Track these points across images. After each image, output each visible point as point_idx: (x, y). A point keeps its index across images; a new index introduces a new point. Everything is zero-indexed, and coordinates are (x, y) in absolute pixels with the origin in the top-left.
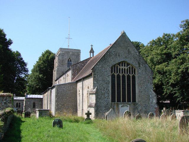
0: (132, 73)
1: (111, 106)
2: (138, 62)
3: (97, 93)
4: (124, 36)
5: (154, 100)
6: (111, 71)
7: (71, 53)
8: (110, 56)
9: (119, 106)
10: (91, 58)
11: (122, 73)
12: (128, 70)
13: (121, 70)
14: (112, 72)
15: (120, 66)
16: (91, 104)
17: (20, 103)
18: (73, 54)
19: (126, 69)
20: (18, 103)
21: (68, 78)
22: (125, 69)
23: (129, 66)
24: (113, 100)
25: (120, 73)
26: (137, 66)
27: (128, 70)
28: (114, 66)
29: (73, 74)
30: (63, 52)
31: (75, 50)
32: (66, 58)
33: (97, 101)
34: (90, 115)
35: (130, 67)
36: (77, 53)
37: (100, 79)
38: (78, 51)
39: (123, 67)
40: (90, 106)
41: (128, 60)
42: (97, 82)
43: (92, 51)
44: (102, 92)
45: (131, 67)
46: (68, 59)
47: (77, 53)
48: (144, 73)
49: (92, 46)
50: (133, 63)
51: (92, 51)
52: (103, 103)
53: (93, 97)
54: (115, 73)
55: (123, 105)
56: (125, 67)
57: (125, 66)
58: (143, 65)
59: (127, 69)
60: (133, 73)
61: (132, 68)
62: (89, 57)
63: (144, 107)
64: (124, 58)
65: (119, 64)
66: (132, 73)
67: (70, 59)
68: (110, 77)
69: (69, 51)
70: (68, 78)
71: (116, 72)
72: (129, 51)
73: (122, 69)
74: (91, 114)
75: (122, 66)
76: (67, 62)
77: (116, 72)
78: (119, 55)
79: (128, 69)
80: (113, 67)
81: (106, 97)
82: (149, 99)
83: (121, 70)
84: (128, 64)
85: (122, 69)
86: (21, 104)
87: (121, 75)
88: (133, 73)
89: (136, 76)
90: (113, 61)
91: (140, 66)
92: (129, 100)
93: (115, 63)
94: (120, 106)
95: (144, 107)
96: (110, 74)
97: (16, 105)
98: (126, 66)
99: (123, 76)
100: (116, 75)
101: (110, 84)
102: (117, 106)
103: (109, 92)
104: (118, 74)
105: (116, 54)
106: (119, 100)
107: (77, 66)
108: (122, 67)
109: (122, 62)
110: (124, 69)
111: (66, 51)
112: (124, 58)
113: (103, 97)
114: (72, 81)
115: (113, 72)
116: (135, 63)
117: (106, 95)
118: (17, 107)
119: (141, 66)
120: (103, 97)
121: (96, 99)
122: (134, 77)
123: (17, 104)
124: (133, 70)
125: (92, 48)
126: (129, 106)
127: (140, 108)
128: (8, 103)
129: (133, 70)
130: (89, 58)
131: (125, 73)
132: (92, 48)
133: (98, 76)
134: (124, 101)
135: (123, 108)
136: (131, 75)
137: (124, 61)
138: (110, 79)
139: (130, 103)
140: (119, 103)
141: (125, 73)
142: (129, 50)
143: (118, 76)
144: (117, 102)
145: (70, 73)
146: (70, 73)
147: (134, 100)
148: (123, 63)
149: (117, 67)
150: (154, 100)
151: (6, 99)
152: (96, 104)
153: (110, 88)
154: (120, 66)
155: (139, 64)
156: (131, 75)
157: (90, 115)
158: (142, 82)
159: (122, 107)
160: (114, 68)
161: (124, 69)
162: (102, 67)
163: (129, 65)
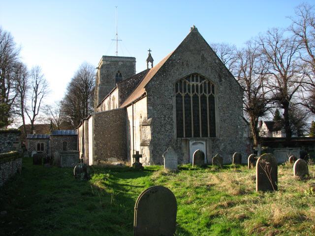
0: (209, 92)
1: (176, 144)
2: (219, 75)
3: (152, 124)
4: (195, 36)
5: (244, 132)
6: (175, 90)
7: (120, 63)
8: (173, 66)
9: (189, 143)
10: (148, 70)
11: (193, 92)
12: (203, 86)
13: (191, 87)
14: (177, 91)
15: (189, 81)
16: (145, 141)
17: (42, 144)
18: (123, 65)
19: (199, 85)
20: (41, 143)
21: (112, 102)
22: (197, 85)
23: (204, 81)
24: (180, 134)
25: (189, 92)
26: (217, 80)
27: (203, 86)
28: (181, 81)
29: (120, 97)
30: (108, 63)
31: (126, 58)
32: (113, 70)
33: (153, 136)
34: (140, 158)
35: (205, 83)
36: (131, 62)
37: (158, 101)
38: (132, 60)
39: (195, 83)
40: (143, 144)
41: (201, 72)
42: (153, 107)
43: (150, 59)
44: (161, 123)
45: (207, 82)
46: (117, 72)
47: (131, 62)
48: (228, 91)
49: (150, 51)
50: (210, 75)
51: (150, 59)
52: (164, 140)
53: (148, 129)
54: (181, 92)
55: (194, 142)
56: (197, 83)
57: (197, 81)
58: (225, 79)
59: (201, 86)
60: (211, 92)
61: (209, 83)
62: (146, 68)
63: (229, 144)
64: (195, 69)
65: (188, 77)
66: (209, 92)
67: (119, 72)
68: (174, 99)
69: (118, 59)
70: (112, 102)
71: (183, 91)
72: (203, 58)
73: (193, 85)
74: (141, 156)
75: (193, 81)
76: (114, 77)
77: (183, 91)
78: (187, 65)
79: (203, 85)
80: (179, 84)
81: (167, 131)
82: (237, 132)
83: (191, 87)
84: (202, 78)
85: (193, 85)
86: (45, 146)
87: (191, 95)
88: (211, 92)
89: (216, 96)
90: (178, 74)
91: (221, 81)
92: (205, 134)
93: (180, 77)
94: (191, 143)
95: (229, 144)
96: (174, 94)
97: (37, 147)
98: (199, 81)
99: (195, 97)
100: (183, 95)
101: (174, 110)
102: (186, 144)
103: (173, 122)
104: (186, 93)
105: (183, 63)
106: (189, 135)
107: (128, 83)
108: (193, 83)
109: (193, 75)
110: (195, 85)
111: (113, 59)
112: (195, 69)
113: (163, 130)
114: (119, 107)
115: (179, 91)
116: (212, 76)
117: (168, 127)
118: (39, 149)
119: (223, 80)
120: (163, 130)
121: (152, 134)
122: (212, 99)
123: (39, 145)
124: (211, 86)
125: (150, 55)
126: (204, 143)
127: (222, 146)
128: (14, 143)
129: (211, 86)
130: (145, 71)
131: (197, 91)
132: (150, 55)
133: (154, 98)
134: (197, 135)
135: (194, 146)
136: (207, 96)
137: (195, 74)
138: (173, 102)
139: (206, 138)
140: (189, 138)
141: (197, 91)
142: (203, 55)
143: (187, 96)
144: (210, 136)
145: (116, 94)
146: (116, 94)
147: (213, 134)
148: (194, 76)
149: (185, 82)
150: (244, 132)
151: (10, 137)
152: (152, 141)
153: (174, 116)
154: (189, 81)
155: (220, 77)
156: (207, 96)
157: (140, 158)
158: (225, 105)
159: (193, 144)
160: (180, 85)
161: (195, 85)
162: (160, 84)
163: (204, 79)
